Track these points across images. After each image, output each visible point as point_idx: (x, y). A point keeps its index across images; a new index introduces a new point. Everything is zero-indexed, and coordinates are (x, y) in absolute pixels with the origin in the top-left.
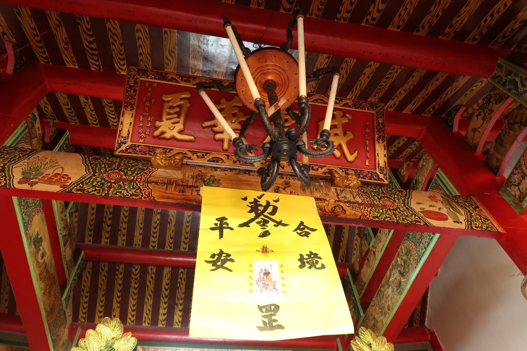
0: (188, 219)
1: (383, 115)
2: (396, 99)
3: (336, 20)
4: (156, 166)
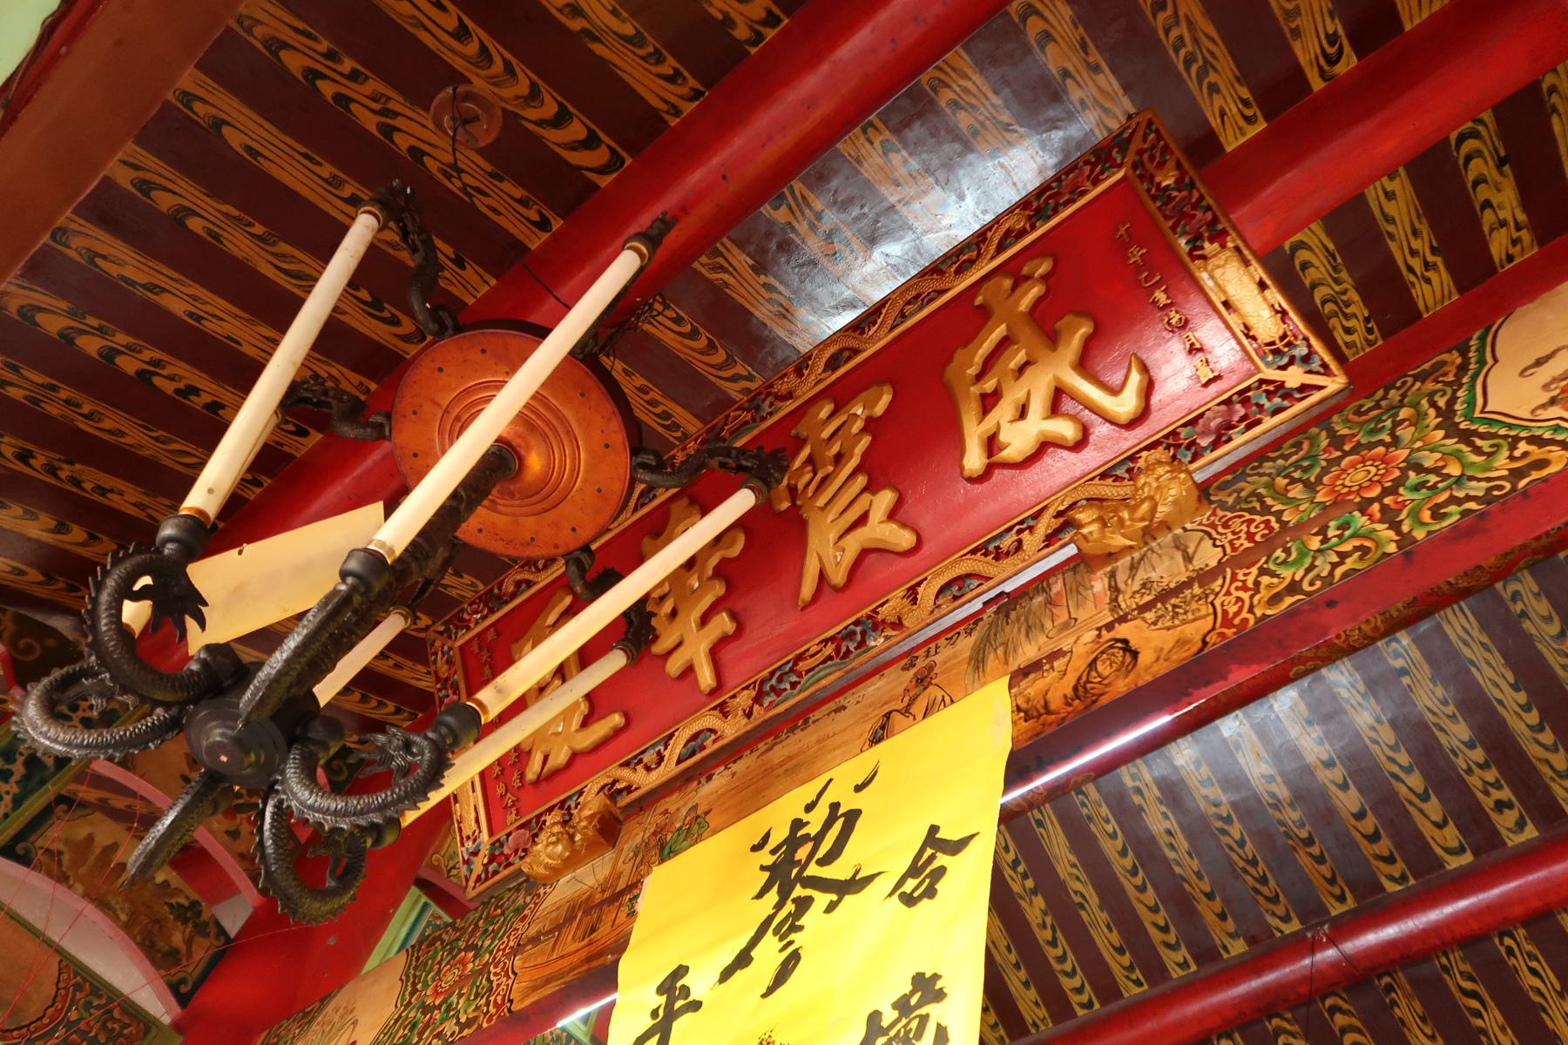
0: (1128, 862)
1: (1166, 149)
2: (1304, 22)
3: (753, 51)
4: (547, 877)
